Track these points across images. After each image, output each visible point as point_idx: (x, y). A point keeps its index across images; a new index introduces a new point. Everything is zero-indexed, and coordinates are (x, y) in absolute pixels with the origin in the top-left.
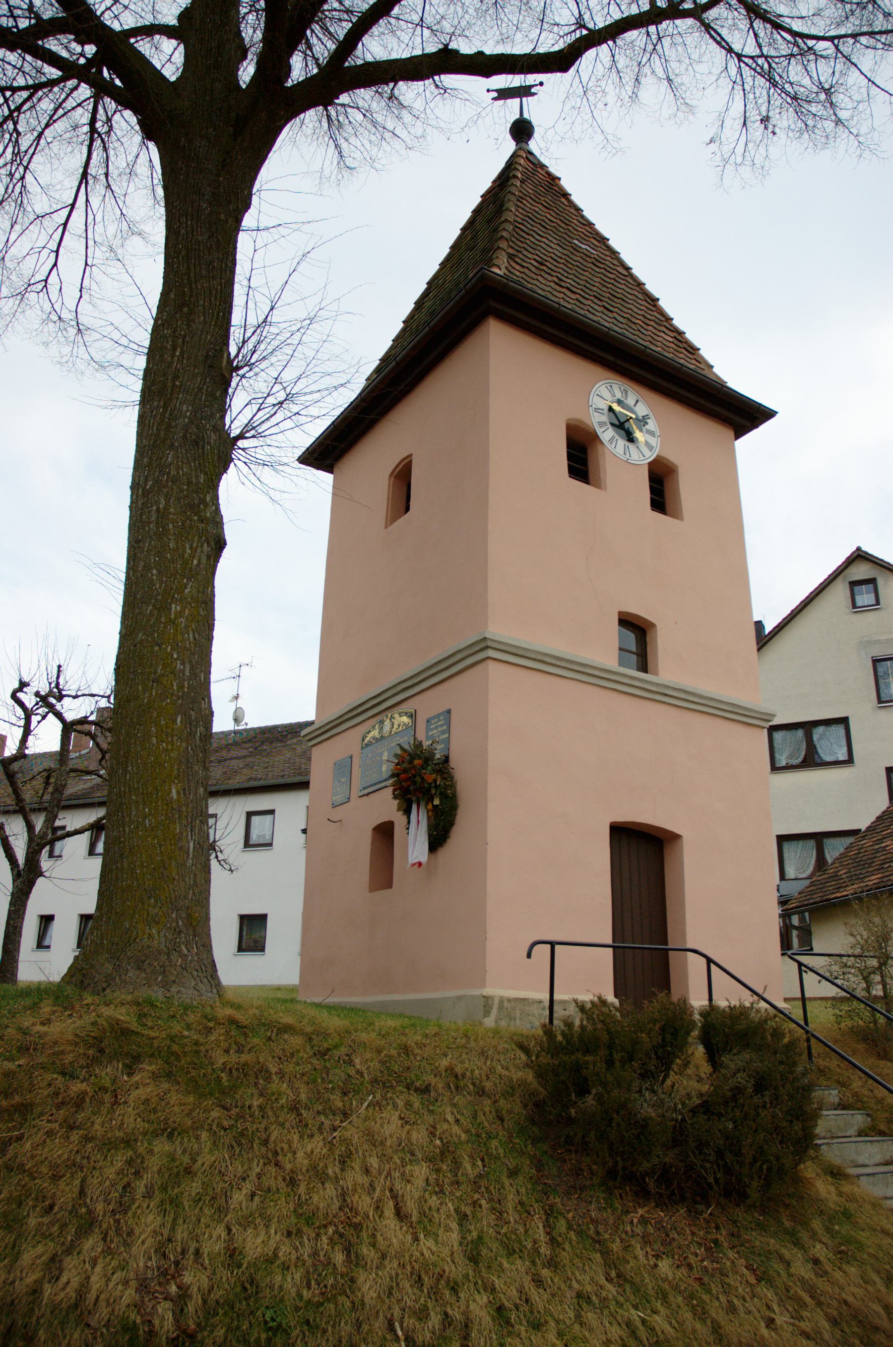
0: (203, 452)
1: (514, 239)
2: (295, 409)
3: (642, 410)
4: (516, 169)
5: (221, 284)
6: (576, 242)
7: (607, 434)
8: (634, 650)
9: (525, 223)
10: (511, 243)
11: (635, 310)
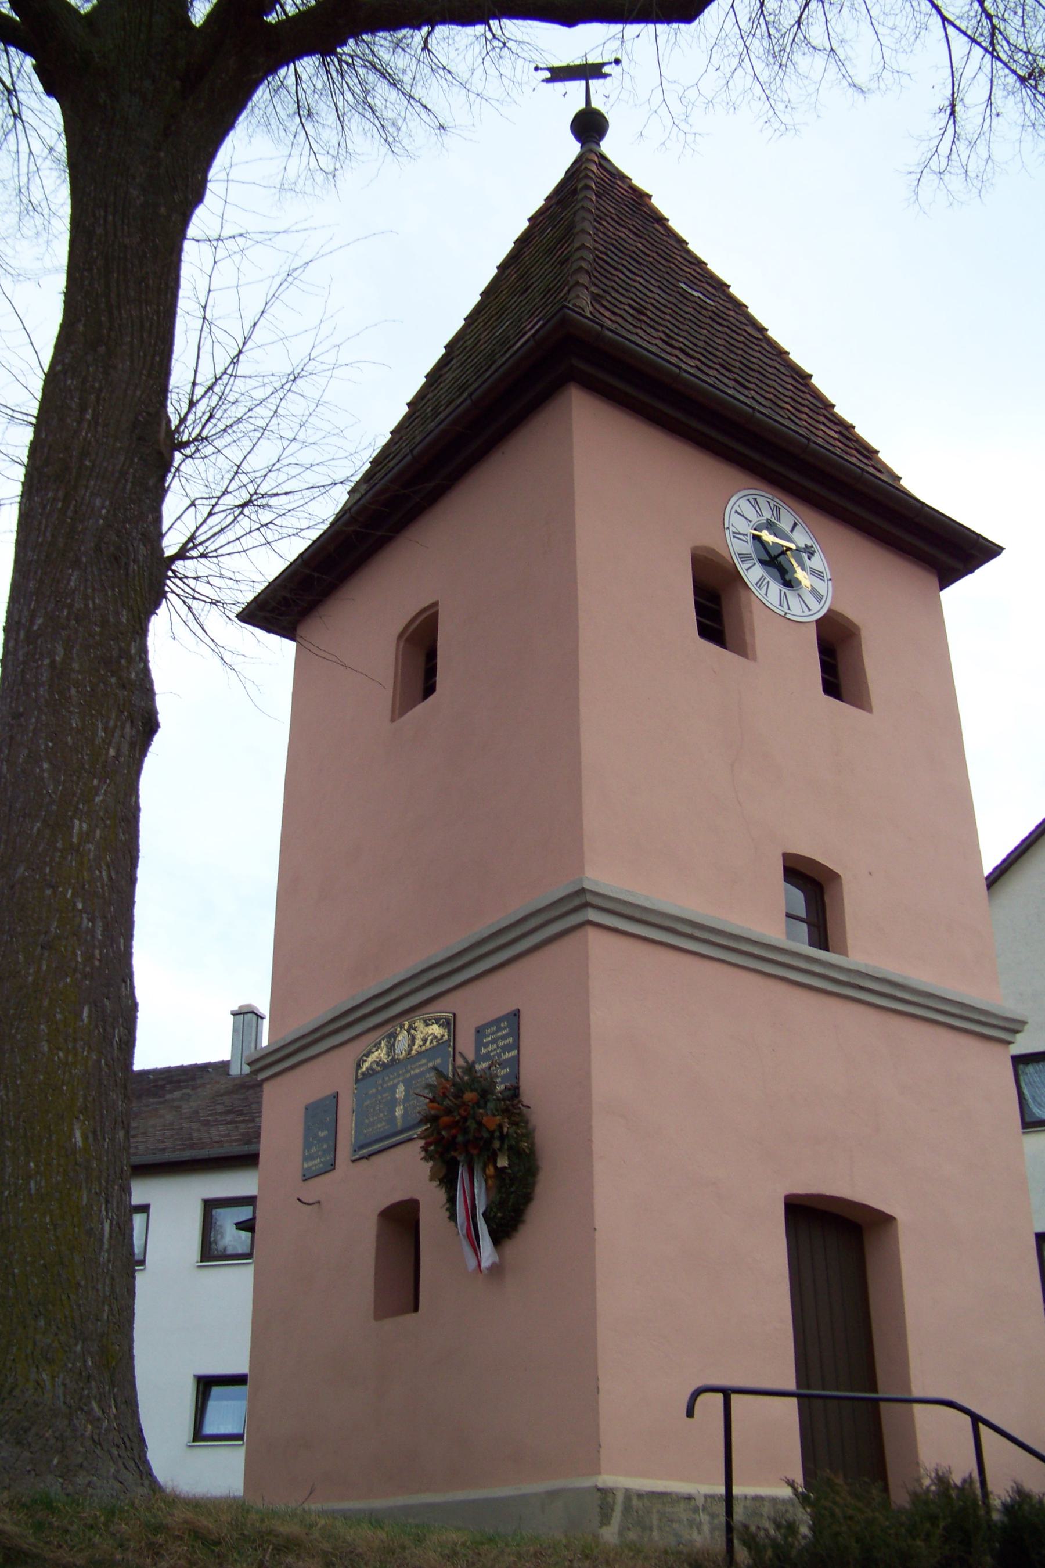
0: (127, 574)
1: (597, 274)
2: (266, 516)
3: (801, 538)
4: (587, 177)
5: (158, 312)
6: (684, 286)
7: (753, 574)
8: (804, 915)
9: (609, 253)
10: (593, 279)
11: (780, 389)
